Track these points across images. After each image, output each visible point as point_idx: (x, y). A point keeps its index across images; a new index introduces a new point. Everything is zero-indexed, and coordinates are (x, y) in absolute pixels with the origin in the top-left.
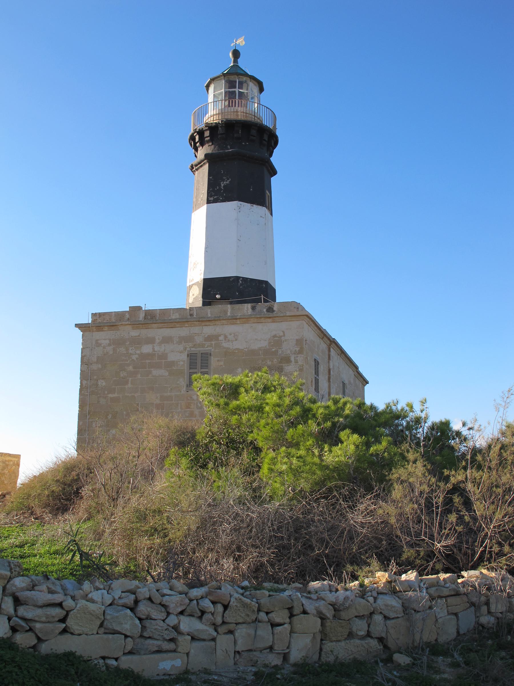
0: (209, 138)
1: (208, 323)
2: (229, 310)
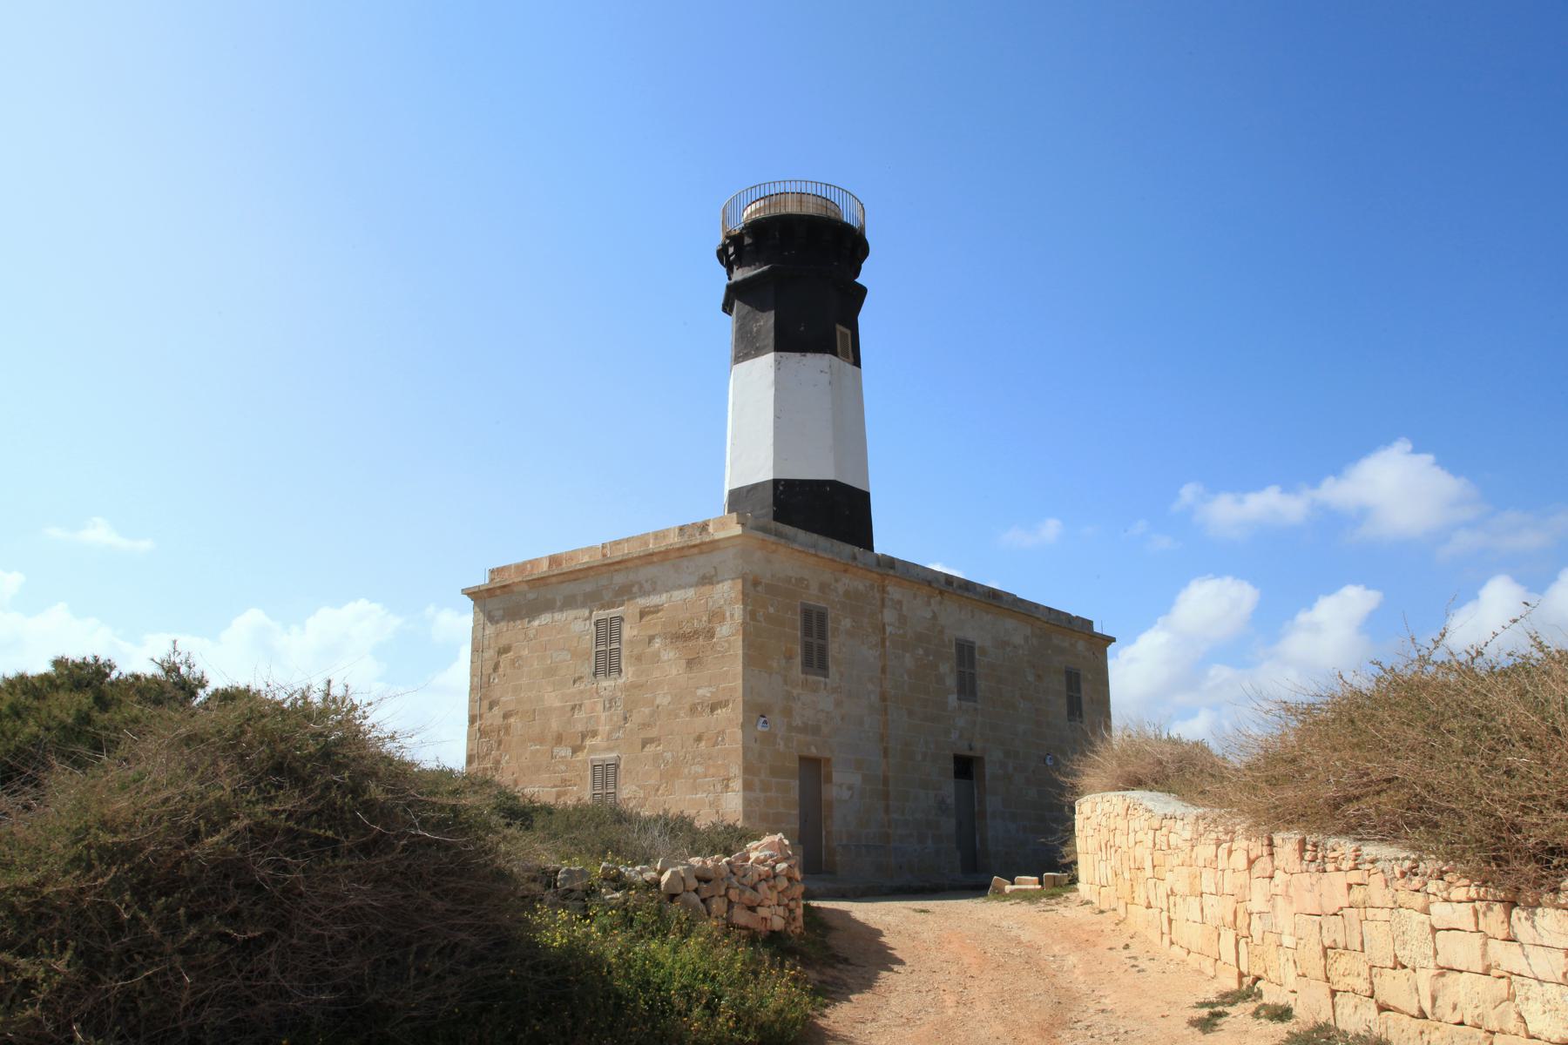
0: (734, 256)
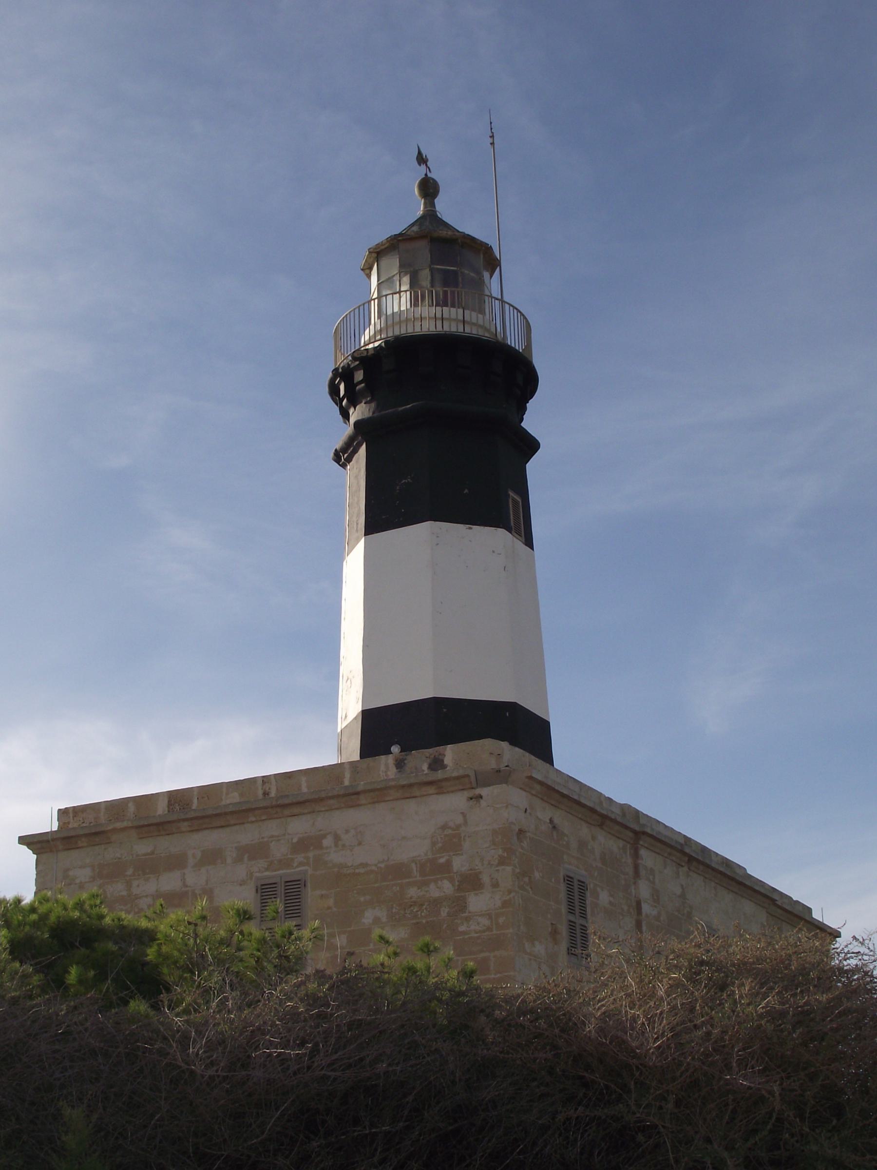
1: (296, 810)
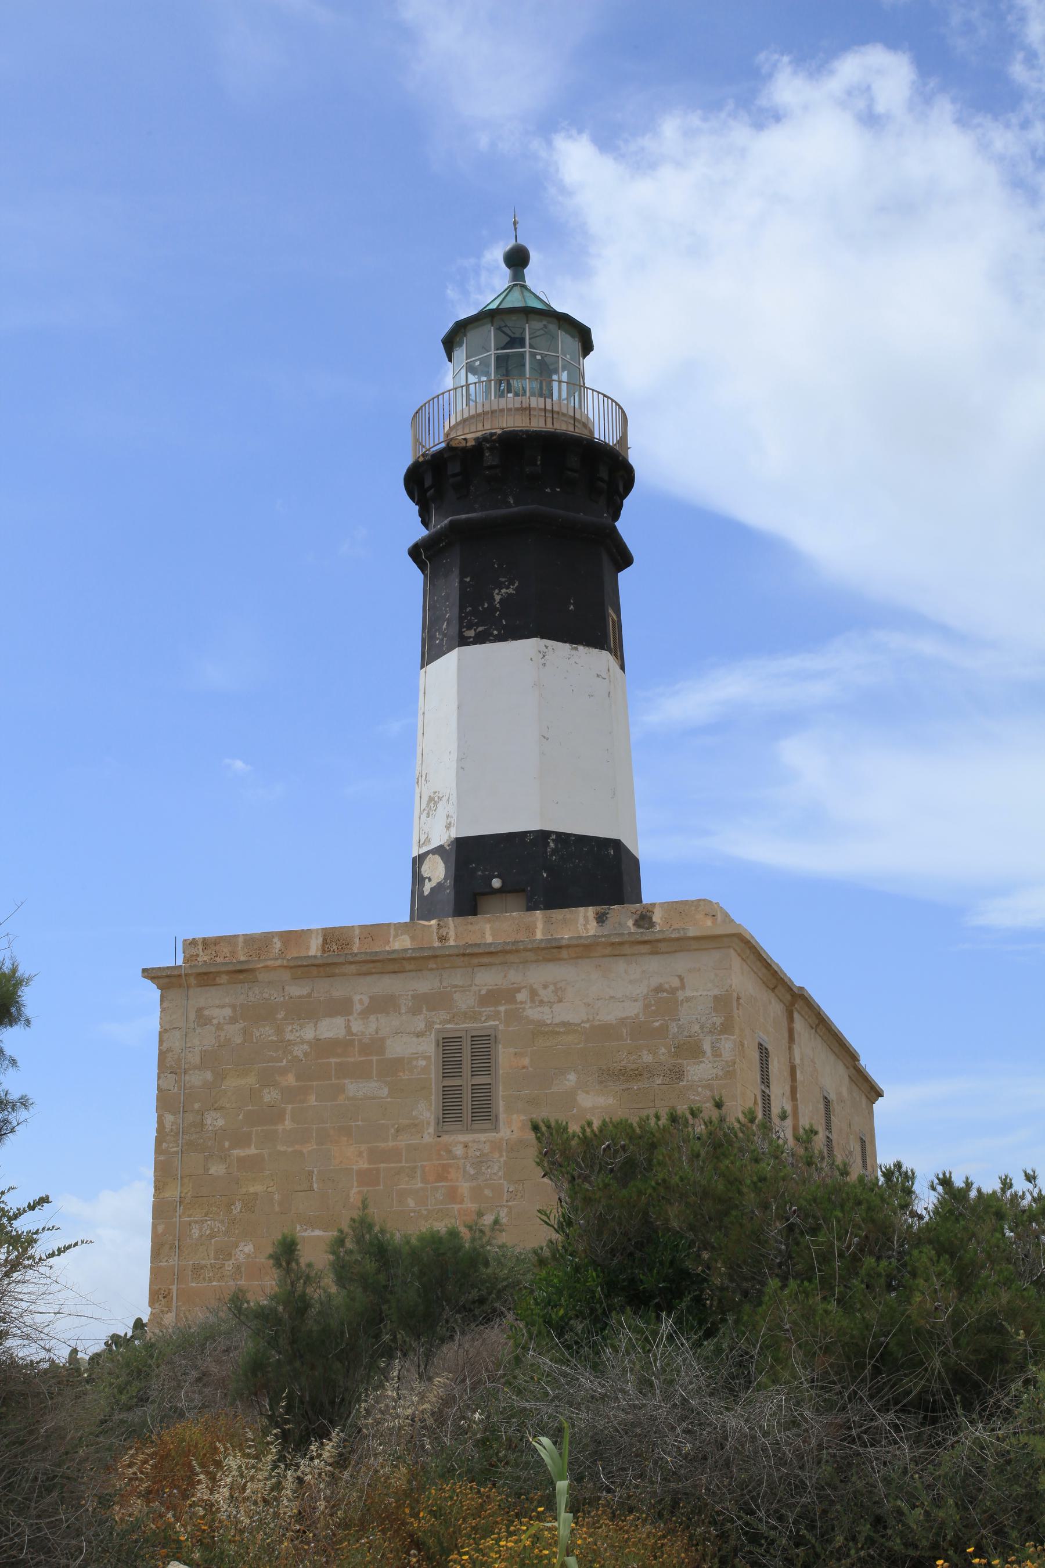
1: (486, 960)
2: (540, 925)
